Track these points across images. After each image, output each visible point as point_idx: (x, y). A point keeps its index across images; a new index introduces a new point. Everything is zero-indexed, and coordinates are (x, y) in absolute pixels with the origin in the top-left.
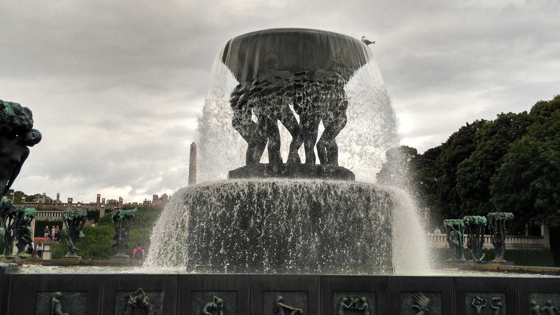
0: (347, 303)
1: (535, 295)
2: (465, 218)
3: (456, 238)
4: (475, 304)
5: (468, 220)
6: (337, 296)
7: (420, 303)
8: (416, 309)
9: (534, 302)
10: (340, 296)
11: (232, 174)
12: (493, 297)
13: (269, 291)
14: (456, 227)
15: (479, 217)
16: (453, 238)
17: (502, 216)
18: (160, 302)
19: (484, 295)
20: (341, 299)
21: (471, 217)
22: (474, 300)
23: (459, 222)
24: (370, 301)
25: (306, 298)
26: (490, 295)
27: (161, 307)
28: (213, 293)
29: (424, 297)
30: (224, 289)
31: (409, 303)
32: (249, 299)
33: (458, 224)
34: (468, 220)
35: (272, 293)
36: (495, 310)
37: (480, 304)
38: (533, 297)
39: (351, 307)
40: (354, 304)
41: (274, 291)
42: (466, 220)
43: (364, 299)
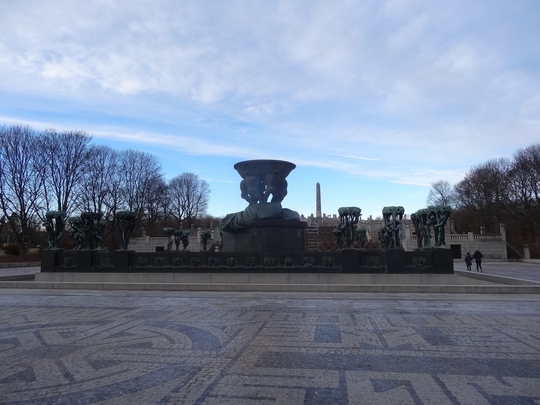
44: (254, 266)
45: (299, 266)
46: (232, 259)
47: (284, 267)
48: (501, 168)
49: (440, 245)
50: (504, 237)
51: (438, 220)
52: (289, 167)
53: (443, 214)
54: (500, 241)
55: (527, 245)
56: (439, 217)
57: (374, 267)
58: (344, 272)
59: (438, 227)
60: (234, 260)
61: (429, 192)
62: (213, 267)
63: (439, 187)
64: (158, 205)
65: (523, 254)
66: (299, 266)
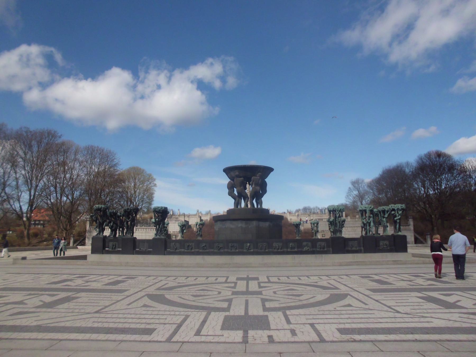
44: (265, 249)
45: (300, 249)
46: (248, 244)
47: (289, 250)
48: (407, 170)
49: (398, 232)
50: (412, 227)
51: (397, 215)
52: (267, 171)
53: (400, 210)
54: (410, 230)
55: (428, 234)
56: (398, 213)
57: (354, 249)
58: (334, 252)
59: (397, 219)
60: (250, 245)
61: (347, 188)
62: (233, 251)
63: (356, 183)
64: (18, 195)
65: (425, 240)
66: (300, 249)
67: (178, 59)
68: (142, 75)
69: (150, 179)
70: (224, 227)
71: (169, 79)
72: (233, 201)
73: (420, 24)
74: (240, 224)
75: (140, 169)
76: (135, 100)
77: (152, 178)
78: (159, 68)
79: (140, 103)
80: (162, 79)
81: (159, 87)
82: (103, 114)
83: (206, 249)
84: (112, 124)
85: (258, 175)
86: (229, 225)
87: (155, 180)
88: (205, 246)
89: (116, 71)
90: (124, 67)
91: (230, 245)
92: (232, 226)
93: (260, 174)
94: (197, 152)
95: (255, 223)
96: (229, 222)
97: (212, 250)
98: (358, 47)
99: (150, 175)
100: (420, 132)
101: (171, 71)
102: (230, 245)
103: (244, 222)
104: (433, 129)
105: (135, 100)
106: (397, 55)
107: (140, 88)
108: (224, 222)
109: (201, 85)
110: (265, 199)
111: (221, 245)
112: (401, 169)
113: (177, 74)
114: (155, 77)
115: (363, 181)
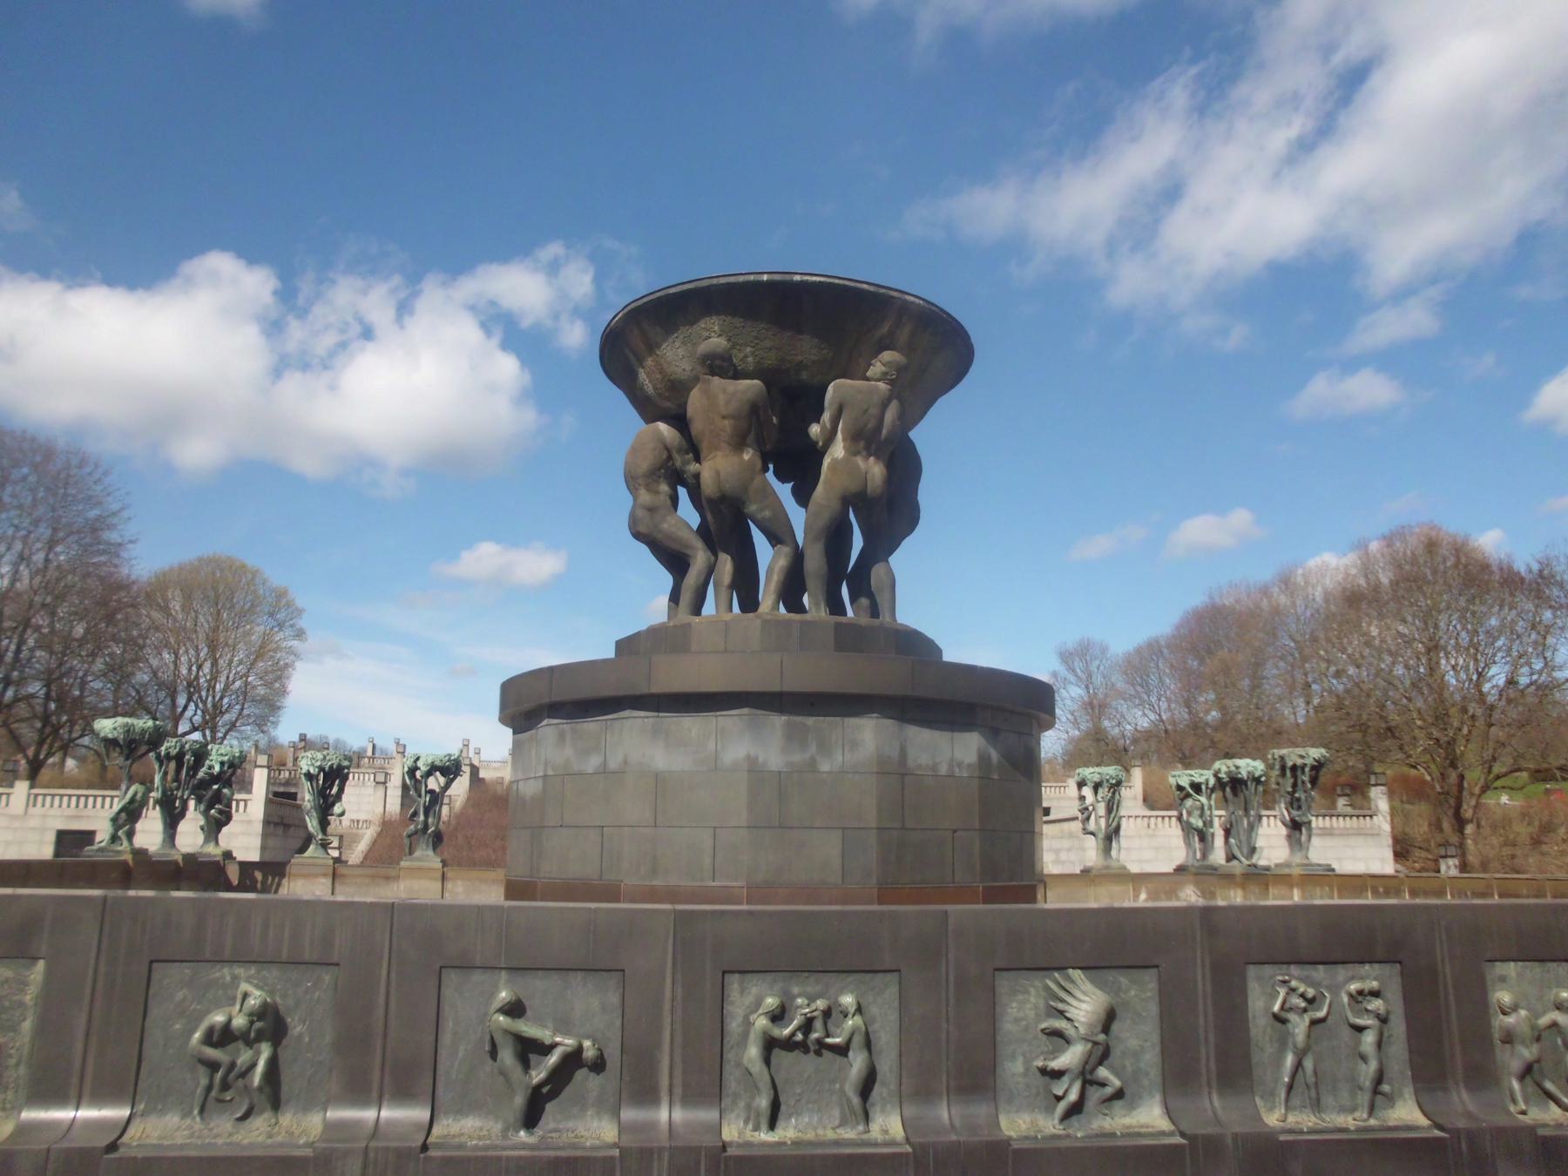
0: (778, 1016)
1: (1511, 969)
2: (1217, 765)
3: (1197, 813)
4: (1282, 1008)
5: (1224, 769)
6: (742, 991)
7: (1072, 1013)
8: (1057, 1034)
9: (1505, 997)
10: (754, 990)
11: (532, 704)
12: (1352, 979)
13: (466, 967)
14: (1197, 787)
15: (1248, 761)
16: (1189, 814)
17: (1302, 757)
18: (21, 1004)
19: (1320, 972)
20: (758, 1003)
21: (1230, 762)
22: (1282, 992)
23: (1204, 776)
24: (874, 1010)
25: (614, 999)
26: (1342, 972)
27: (27, 1025)
28: (239, 971)
29: (1088, 986)
30: (284, 957)
31: (1031, 1014)
32: (381, 1000)
33: (1201, 780)
34: (1224, 769)
35: (477, 977)
36: (1360, 1029)
37: (1305, 1010)
38: (1503, 979)
39: (793, 1034)
40: (807, 1026)
41: (485, 968)
42: (1219, 771)
43: (848, 1000)
60: (1109, 1019)
67: (433, 243)
68: (306, 287)
69: (281, 609)
70: (593, 763)
71: (404, 309)
72: (666, 579)
73: (1202, 191)
74: (742, 744)
75: (243, 566)
76: (280, 368)
77: (288, 605)
78: (369, 267)
79: (293, 385)
80: (377, 304)
81: (368, 334)
82: (171, 414)
83: (274, 1093)
84: (197, 452)
85: (876, 368)
86: (634, 742)
87: (300, 612)
88: (270, 1024)
89: (221, 263)
90: (251, 255)
91: (753, 1006)
92: (661, 759)
93: (887, 356)
94: (484, 558)
95: (868, 735)
96: (634, 723)
97: (403, 1115)
98: (1015, 246)
99: (281, 594)
100: (1200, 530)
101: (414, 279)
102: (753, 1006)
103: (779, 721)
104: (1241, 518)
105: (280, 368)
106: (1131, 283)
107: (296, 332)
108: (591, 725)
109: (505, 327)
110: (909, 566)
111: (575, 1018)
112: (1431, 546)
113: (433, 295)
114: (353, 297)
115: (1104, 650)
